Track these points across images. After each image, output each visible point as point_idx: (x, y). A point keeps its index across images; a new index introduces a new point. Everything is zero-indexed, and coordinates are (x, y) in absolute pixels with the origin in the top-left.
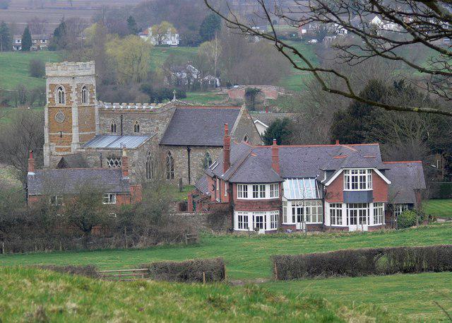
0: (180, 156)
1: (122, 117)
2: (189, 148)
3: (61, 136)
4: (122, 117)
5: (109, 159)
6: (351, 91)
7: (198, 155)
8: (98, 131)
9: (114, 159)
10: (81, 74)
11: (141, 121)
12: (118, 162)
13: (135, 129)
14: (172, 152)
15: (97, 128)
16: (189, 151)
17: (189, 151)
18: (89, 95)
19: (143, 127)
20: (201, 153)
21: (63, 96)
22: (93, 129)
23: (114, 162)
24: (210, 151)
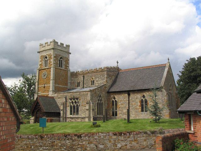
0: (121, 100)
1: (84, 76)
2: (129, 92)
3: (44, 87)
4: (84, 76)
5: (71, 99)
6: (163, 122)
7: (136, 98)
8: (69, 87)
9: (74, 99)
10: (59, 49)
11: (96, 78)
12: (77, 101)
13: (92, 83)
14: (116, 97)
15: (69, 84)
16: (129, 95)
17: (129, 95)
18: (64, 63)
19: (97, 81)
20: (139, 96)
21: (47, 61)
22: (66, 84)
23: (74, 101)
24: (146, 94)
